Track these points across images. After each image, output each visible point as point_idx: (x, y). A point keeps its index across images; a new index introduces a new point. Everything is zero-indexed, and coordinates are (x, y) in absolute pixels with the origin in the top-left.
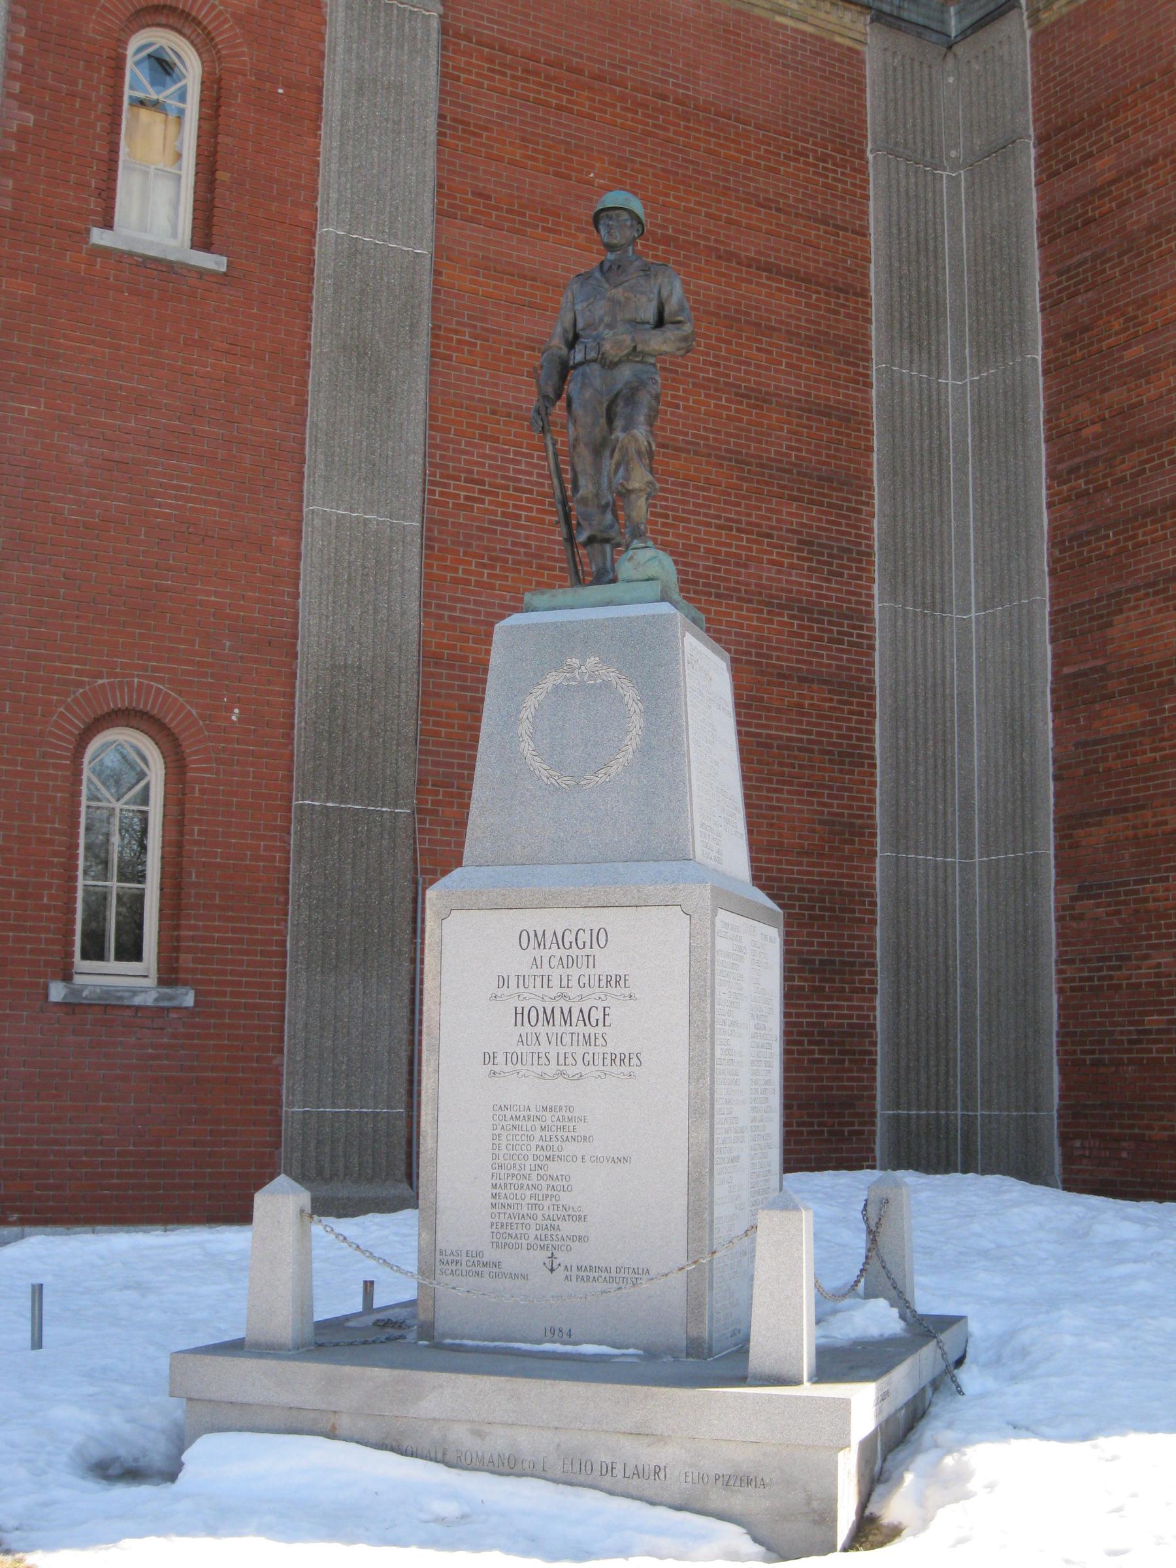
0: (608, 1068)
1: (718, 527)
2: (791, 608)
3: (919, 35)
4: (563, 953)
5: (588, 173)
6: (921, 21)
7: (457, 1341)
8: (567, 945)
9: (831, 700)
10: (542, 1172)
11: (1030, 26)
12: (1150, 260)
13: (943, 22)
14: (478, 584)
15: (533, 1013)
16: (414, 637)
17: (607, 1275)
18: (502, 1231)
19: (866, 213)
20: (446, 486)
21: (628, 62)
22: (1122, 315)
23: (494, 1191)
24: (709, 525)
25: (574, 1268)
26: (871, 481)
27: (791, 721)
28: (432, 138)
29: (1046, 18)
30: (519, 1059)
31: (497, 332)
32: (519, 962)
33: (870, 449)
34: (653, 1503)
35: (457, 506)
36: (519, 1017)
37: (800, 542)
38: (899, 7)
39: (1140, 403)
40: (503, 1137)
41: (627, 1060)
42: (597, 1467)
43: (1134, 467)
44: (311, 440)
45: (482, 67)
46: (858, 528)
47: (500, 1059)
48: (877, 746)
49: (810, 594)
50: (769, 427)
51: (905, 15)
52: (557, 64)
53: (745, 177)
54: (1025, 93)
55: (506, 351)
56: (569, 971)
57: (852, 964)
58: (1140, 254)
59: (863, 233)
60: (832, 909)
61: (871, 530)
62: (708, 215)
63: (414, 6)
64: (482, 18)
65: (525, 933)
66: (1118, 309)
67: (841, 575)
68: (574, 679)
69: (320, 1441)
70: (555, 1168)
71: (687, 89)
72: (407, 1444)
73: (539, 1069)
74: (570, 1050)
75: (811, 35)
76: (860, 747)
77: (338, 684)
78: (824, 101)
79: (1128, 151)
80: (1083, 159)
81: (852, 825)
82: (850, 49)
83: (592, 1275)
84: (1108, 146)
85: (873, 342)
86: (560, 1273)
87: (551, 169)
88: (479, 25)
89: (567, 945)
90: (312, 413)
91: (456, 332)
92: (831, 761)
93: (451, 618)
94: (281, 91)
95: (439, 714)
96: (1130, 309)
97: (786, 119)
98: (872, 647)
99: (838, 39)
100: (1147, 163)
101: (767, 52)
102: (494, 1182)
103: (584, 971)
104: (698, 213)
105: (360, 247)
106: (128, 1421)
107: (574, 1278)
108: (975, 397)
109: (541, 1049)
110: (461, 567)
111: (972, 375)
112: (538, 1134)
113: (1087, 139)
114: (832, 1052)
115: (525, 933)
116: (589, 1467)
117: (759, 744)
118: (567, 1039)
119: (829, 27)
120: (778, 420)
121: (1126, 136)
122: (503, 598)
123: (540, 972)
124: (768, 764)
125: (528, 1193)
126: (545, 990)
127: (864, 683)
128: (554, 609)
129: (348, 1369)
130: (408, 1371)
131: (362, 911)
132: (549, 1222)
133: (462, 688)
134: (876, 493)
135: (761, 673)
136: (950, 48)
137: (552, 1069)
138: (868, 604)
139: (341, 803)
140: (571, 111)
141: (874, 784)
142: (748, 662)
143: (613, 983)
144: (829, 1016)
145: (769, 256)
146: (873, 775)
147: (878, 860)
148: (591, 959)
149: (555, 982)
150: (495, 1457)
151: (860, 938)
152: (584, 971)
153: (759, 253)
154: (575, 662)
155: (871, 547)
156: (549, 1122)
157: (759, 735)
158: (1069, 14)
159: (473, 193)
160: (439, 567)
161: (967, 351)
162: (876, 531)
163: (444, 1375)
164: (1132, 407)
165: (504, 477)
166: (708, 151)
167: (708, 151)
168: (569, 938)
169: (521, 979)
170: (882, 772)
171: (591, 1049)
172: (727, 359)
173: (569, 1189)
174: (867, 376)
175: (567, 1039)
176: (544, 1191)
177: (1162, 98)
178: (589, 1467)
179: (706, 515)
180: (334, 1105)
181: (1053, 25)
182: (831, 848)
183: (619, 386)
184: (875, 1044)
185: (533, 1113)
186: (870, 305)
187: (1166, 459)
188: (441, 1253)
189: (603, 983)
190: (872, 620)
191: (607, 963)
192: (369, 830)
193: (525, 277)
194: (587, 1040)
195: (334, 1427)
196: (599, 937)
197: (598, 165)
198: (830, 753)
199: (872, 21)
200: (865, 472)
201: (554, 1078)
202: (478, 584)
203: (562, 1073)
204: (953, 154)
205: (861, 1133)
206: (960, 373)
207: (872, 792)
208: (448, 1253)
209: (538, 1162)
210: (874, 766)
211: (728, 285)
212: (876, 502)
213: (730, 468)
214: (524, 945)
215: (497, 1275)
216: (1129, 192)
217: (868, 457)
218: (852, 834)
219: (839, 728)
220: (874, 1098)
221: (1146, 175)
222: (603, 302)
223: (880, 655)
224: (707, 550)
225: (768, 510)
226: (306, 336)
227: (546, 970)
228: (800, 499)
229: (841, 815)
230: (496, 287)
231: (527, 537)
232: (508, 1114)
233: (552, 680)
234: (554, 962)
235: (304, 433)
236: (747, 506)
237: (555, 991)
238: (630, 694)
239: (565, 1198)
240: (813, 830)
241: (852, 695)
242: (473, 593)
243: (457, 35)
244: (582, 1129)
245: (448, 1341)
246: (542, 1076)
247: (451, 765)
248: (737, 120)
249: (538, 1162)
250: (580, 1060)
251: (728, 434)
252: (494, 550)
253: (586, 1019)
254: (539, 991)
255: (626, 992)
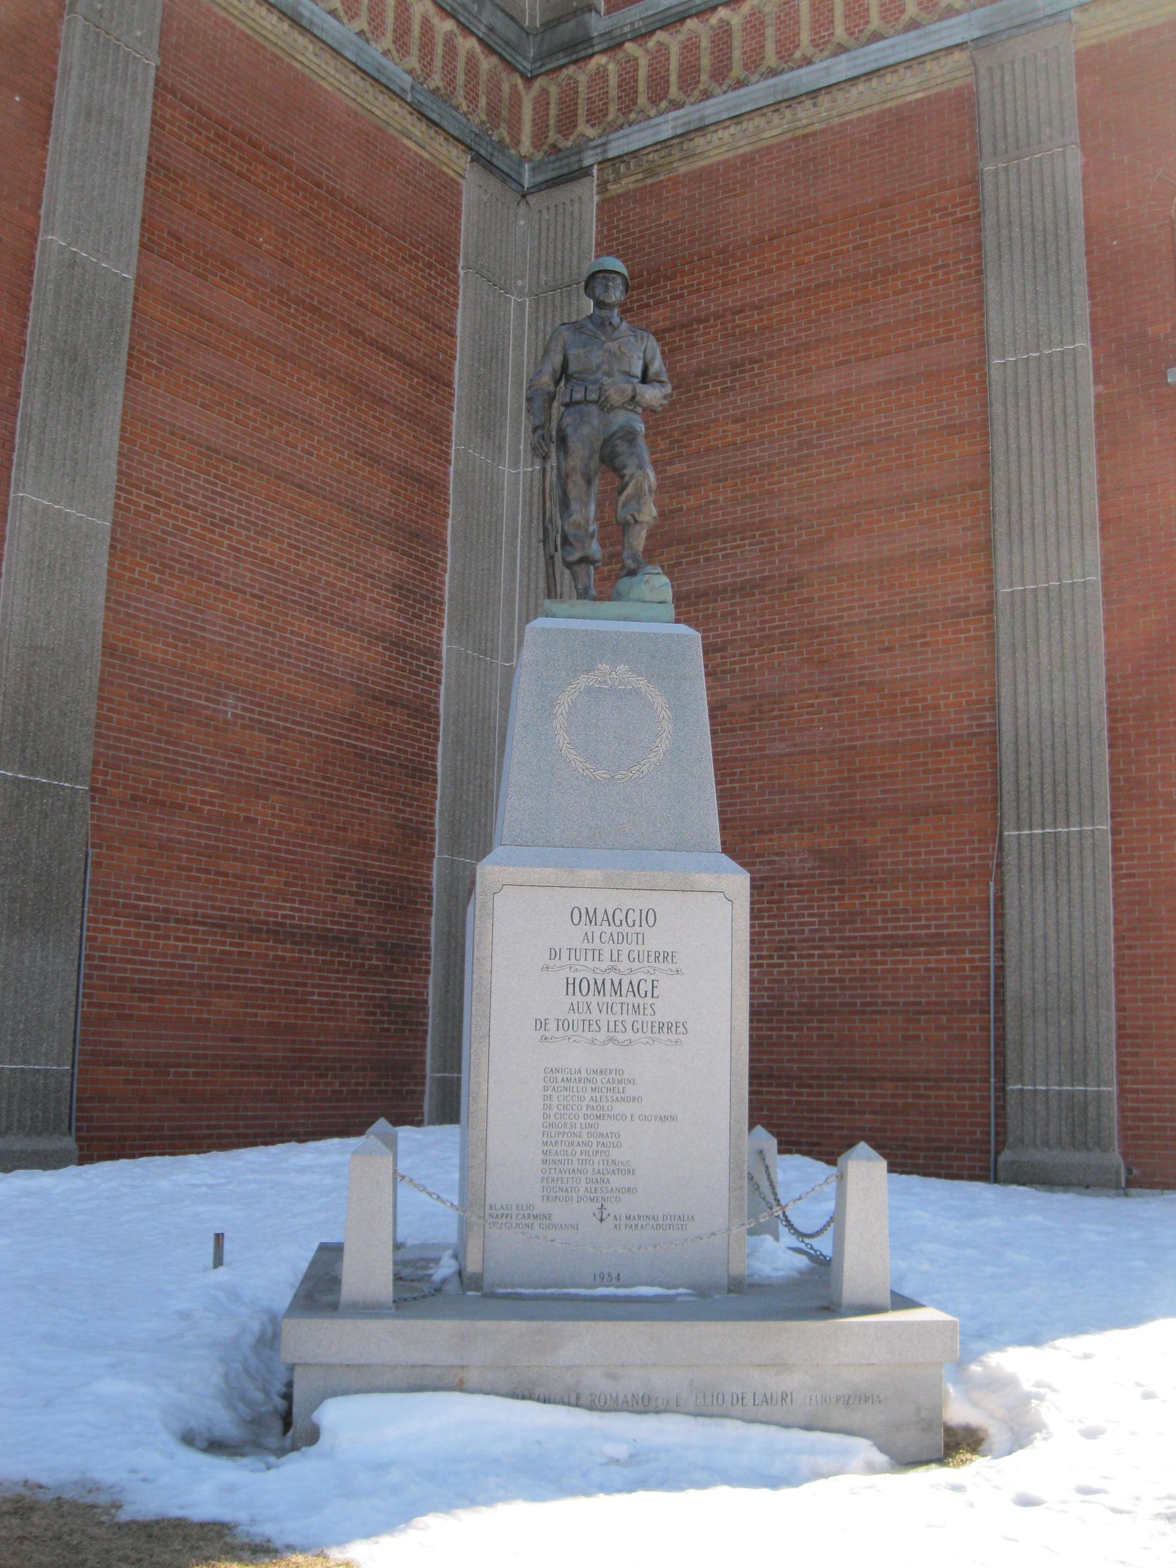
0: (657, 1036)
1: (337, 563)
2: (384, 641)
3: (504, 181)
4: (614, 929)
5: (258, 238)
6: (505, 169)
7: (510, 1290)
8: (618, 923)
9: (408, 723)
10: (592, 1130)
11: (598, 193)
12: (698, 397)
13: (520, 174)
14: (151, 586)
15: (585, 984)
16: (100, 628)
17: (654, 1223)
18: (552, 1185)
19: (455, 318)
20: (130, 493)
21: (294, 149)
22: (668, 437)
23: (545, 1148)
24: (329, 560)
25: (623, 1217)
26: (445, 542)
27: (379, 737)
28: (143, 175)
29: (614, 190)
30: (571, 1025)
31: (179, 362)
32: (573, 936)
33: (446, 515)
34: (787, 1426)
35: (137, 513)
36: (571, 987)
37: (394, 585)
38: (492, 155)
39: (681, 509)
40: (555, 1098)
41: (674, 1029)
42: (728, 1398)
43: (672, 559)
44: (22, 430)
45: (183, 123)
46: (434, 580)
47: (552, 1025)
48: (439, 764)
49: (398, 631)
50: (378, 484)
51: (495, 161)
52: (241, 135)
53: (372, 269)
54: (590, 246)
55: (186, 381)
56: (619, 947)
57: (414, 948)
58: (689, 391)
59: (452, 334)
60: (402, 901)
61: (443, 583)
62: (344, 294)
63: (137, 52)
64: (186, 79)
65: (576, 911)
66: (664, 432)
67: (421, 617)
68: (605, 682)
69: (456, 1396)
70: (605, 1126)
71: (336, 183)
72: (540, 1391)
73: (590, 1035)
74: (620, 1018)
75: (427, 161)
76: (427, 765)
77: (34, 663)
78: (432, 218)
79: (683, 308)
80: (639, 307)
81: (418, 829)
82: (452, 180)
83: (640, 1223)
84: (664, 301)
85: (454, 427)
86: (609, 1221)
87: (231, 226)
88: (183, 85)
89: (618, 923)
90: (25, 406)
91: (147, 355)
92: (407, 775)
93: (127, 614)
94: (18, 99)
95: (112, 701)
96: (676, 433)
97: (404, 227)
98: (439, 681)
99: (445, 169)
100: (699, 321)
101: (395, 167)
102: (545, 1139)
103: (633, 947)
104: (337, 290)
105: (78, 260)
106: (181, 1390)
107: (623, 1227)
108: (527, 485)
109: (591, 1017)
110: (137, 569)
111: (525, 466)
112: (588, 1096)
113: (645, 292)
114: (396, 1023)
115: (576, 911)
116: (720, 1399)
117: (356, 755)
118: (617, 1008)
119: (441, 157)
120: (384, 480)
121: (682, 296)
122: (169, 601)
123: (591, 946)
124: (361, 772)
125: (578, 1149)
126: (596, 964)
127: (432, 710)
128: (573, 617)
129: (481, 1324)
130: (545, 1322)
131: (43, 878)
132: (598, 1177)
133: (132, 679)
134: (449, 553)
135: (361, 694)
136: (524, 196)
137: (602, 1035)
138: (438, 645)
139: (33, 775)
140: (249, 180)
141: (435, 796)
142: (351, 683)
143: (661, 958)
144: (396, 992)
145: (385, 339)
146: (435, 789)
147: (435, 861)
148: (640, 937)
149: (606, 956)
150: (629, 1398)
151: (419, 926)
152: (633, 947)
153: (379, 335)
154: (605, 667)
155: (442, 596)
156: (599, 1084)
157: (356, 747)
158: (635, 190)
159: (169, 233)
160: (120, 566)
161: (522, 447)
162: (447, 584)
163: (583, 1323)
164: (671, 511)
165: (176, 493)
166: (347, 239)
167: (347, 239)
168: (620, 916)
169: (573, 952)
170: (442, 786)
171: (640, 1018)
172: (350, 421)
173: (619, 1145)
174: (448, 454)
175: (617, 1008)
176: (595, 1147)
177: (717, 272)
178: (720, 1399)
179: (328, 552)
180: (11, 1062)
181: (619, 196)
182: (403, 848)
183: (615, 428)
184: (426, 1016)
185: (584, 1075)
186: (453, 395)
187: (702, 557)
188: (491, 1207)
189: (652, 959)
190: (440, 659)
191: (656, 940)
192: (53, 804)
193: (203, 317)
194: (636, 1009)
195: (461, 1382)
196: (648, 917)
197: (266, 231)
198: (406, 767)
199: (472, 160)
200: (442, 534)
201: (604, 1043)
202: (151, 586)
203: (612, 1039)
204: (520, 283)
205: (414, 1092)
206: (515, 464)
207: (433, 803)
208: (498, 1206)
209: (588, 1121)
210: (435, 781)
211: (355, 357)
212: (449, 560)
213: (347, 514)
214: (576, 921)
215: (548, 1227)
216: (681, 340)
217: (444, 521)
218: (419, 837)
219: (413, 746)
220: (424, 1062)
221: (699, 330)
222: (600, 352)
223: (446, 689)
224: (327, 583)
225: (373, 555)
226: (23, 333)
227: (597, 944)
228: (396, 550)
229: (410, 820)
230: (181, 321)
231: (191, 550)
232: (559, 1076)
233: (583, 680)
234: (605, 938)
235: (15, 423)
236: (358, 549)
237: (604, 966)
238: (659, 701)
239: (614, 1154)
240: (392, 832)
241: (423, 720)
242: (144, 593)
243: (165, 88)
244: (631, 1091)
245: (501, 1290)
246: (593, 1042)
247: (119, 749)
248: (370, 219)
249: (588, 1121)
250: (629, 1028)
251: (347, 485)
252: (165, 557)
253: (635, 990)
254: (590, 964)
255: (674, 967)
